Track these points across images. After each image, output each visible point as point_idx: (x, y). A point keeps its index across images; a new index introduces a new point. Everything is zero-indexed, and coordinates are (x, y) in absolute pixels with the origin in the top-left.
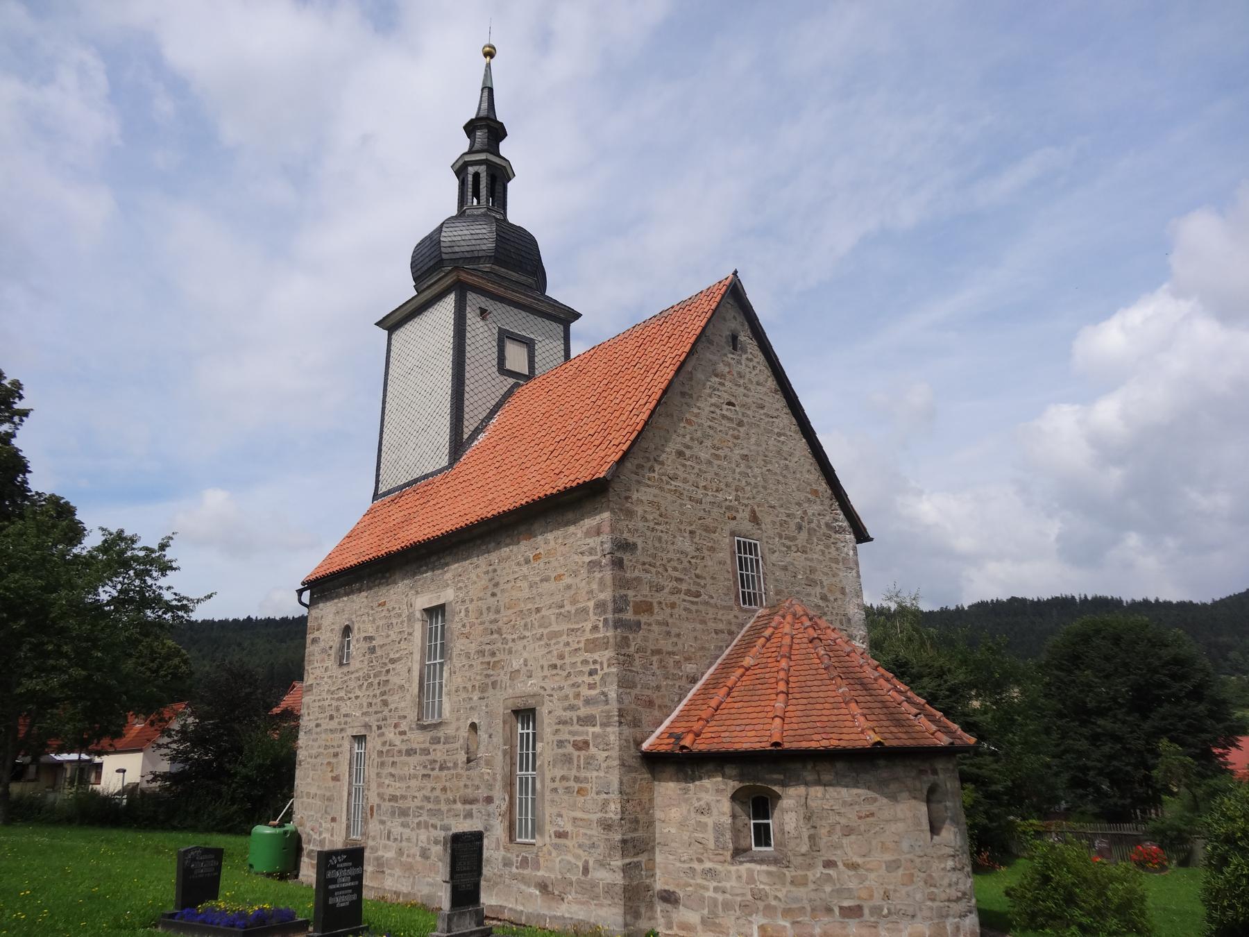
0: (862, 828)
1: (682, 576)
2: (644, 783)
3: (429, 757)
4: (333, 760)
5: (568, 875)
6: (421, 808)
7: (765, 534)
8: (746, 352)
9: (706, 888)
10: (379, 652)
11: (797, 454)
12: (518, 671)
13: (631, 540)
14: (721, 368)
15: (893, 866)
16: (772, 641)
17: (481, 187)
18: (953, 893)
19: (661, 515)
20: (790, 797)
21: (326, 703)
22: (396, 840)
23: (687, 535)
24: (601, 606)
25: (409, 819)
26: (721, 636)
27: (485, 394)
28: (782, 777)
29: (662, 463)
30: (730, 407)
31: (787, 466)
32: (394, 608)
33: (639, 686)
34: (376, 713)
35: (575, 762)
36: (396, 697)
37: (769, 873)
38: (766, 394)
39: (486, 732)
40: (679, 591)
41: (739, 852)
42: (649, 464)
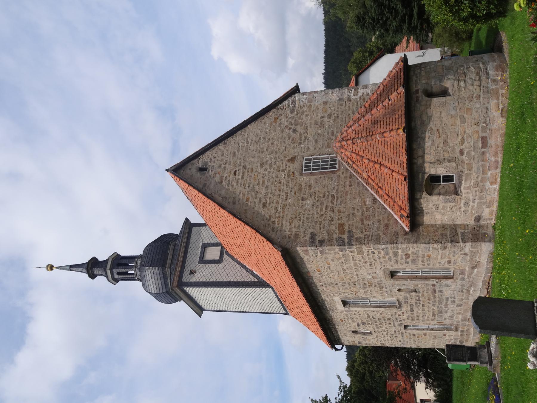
0: (445, 136)
1: (325, 205)
2: (424, 230)
3: (414, 304)
4: (417, 336)
5: (468, 260)
6: (438, 307)
7: (300, 153)
8: (207, 162)
9: (473, 207)
10: (365, 321)
11: (256, 131)
12: (373, 276)
13: (309, 236)
14: (217, 179)
15: (463, 120)
16: (355, 161)
17: (124, 271)
18: (476, 83)
19: (296, 218)
20: (430, 171)
21: (389, 338)
22: (453, 315)
23: (304, 202)
24: (341, 250)
25: (443, 311)
26: (353, 183)
27: (233, 270)
28: (420, 175)
29: (270, 216)
30: (237, 174)
31: (264, 138)
32: (344, 317)
33: (379, 232)
34: (393, 322)
35: (415, 258)
36: (386, 316)
37: (466, 180)
38: (227, 150)
39: (401, 286)
40: (332, 207)
41: (456, 192)
42: (271, 224)
